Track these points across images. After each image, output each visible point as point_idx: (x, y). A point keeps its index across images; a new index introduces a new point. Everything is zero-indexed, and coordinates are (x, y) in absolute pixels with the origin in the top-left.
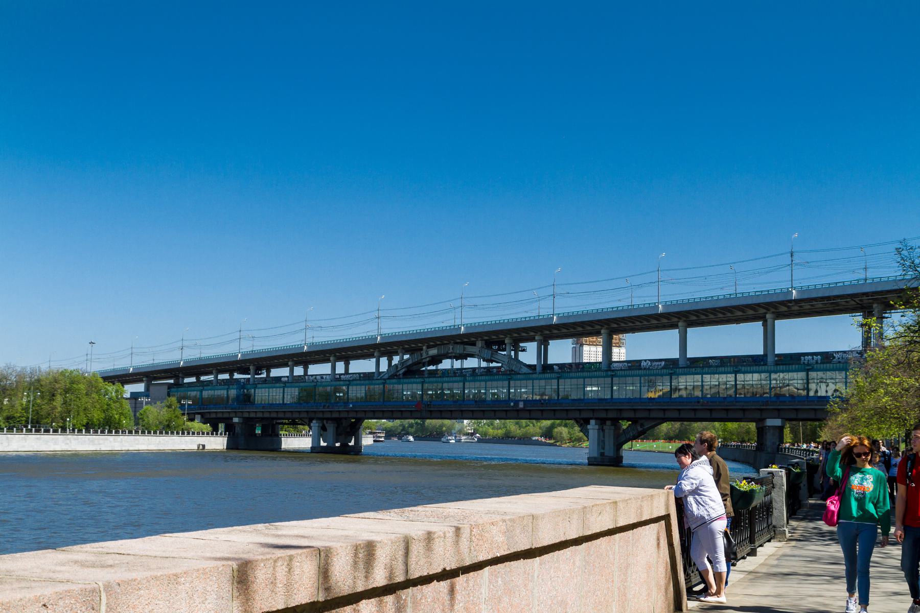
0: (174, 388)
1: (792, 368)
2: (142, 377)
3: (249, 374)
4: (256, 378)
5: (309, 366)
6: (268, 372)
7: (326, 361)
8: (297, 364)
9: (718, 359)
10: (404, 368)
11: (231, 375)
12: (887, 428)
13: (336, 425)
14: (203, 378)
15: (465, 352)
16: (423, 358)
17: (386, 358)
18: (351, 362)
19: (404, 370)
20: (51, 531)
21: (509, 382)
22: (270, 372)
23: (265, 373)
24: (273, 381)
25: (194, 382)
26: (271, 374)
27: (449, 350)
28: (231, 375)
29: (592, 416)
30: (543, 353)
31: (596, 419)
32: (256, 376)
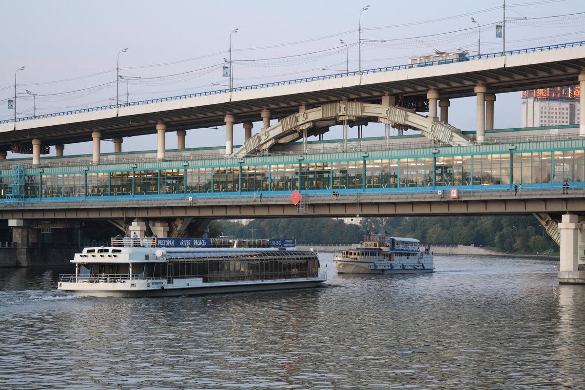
10: (270, 140)
13: (168, 229)
15: (364, 114)
16: (299, 123)
19: (270, 143)
22: (252, 126)
27: (340, 111)
29: (564, 209)
31: (572, 213)
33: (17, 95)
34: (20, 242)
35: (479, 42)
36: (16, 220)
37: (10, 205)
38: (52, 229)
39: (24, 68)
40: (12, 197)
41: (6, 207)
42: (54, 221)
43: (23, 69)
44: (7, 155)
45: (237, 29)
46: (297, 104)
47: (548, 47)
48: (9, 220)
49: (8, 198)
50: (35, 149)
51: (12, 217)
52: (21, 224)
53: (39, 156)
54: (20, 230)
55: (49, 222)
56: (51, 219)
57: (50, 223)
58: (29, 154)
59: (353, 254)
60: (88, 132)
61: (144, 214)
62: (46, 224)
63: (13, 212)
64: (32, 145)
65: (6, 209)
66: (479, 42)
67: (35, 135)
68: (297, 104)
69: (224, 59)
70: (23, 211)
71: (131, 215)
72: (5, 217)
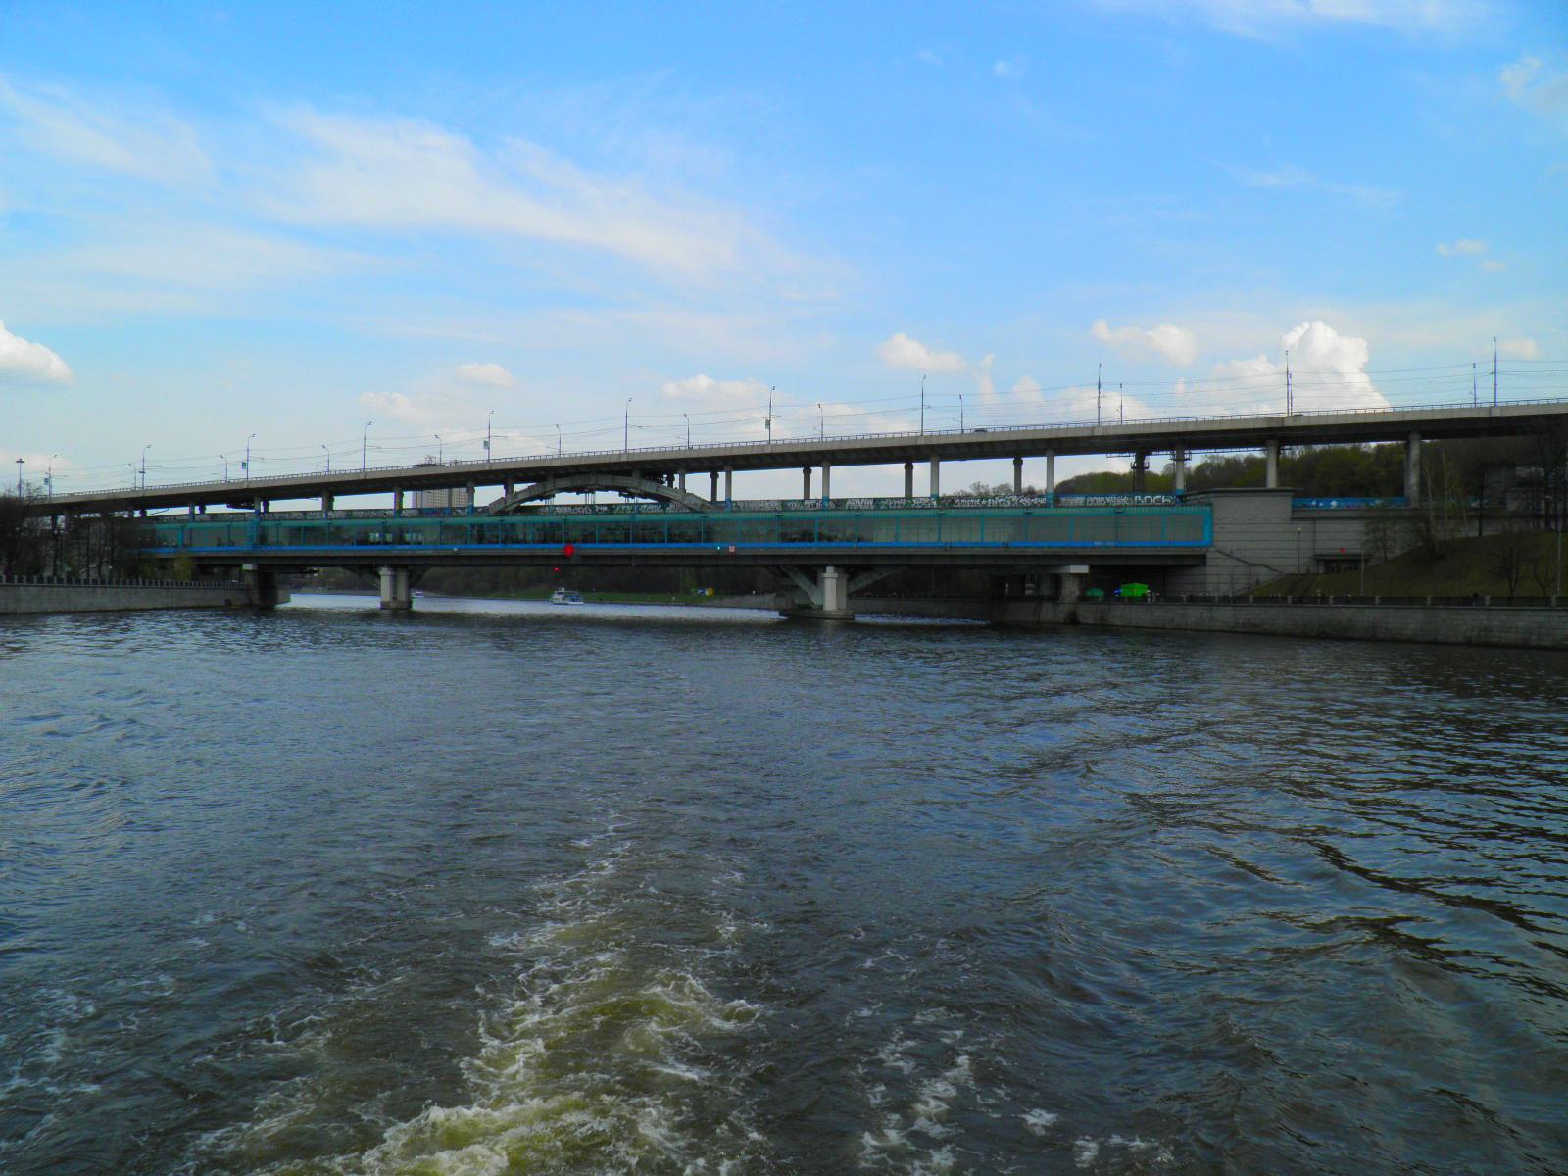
22: (333, 500)
31: (833, 566)
61: (395, 562)
63: (247, 559)
71: (824, 562)
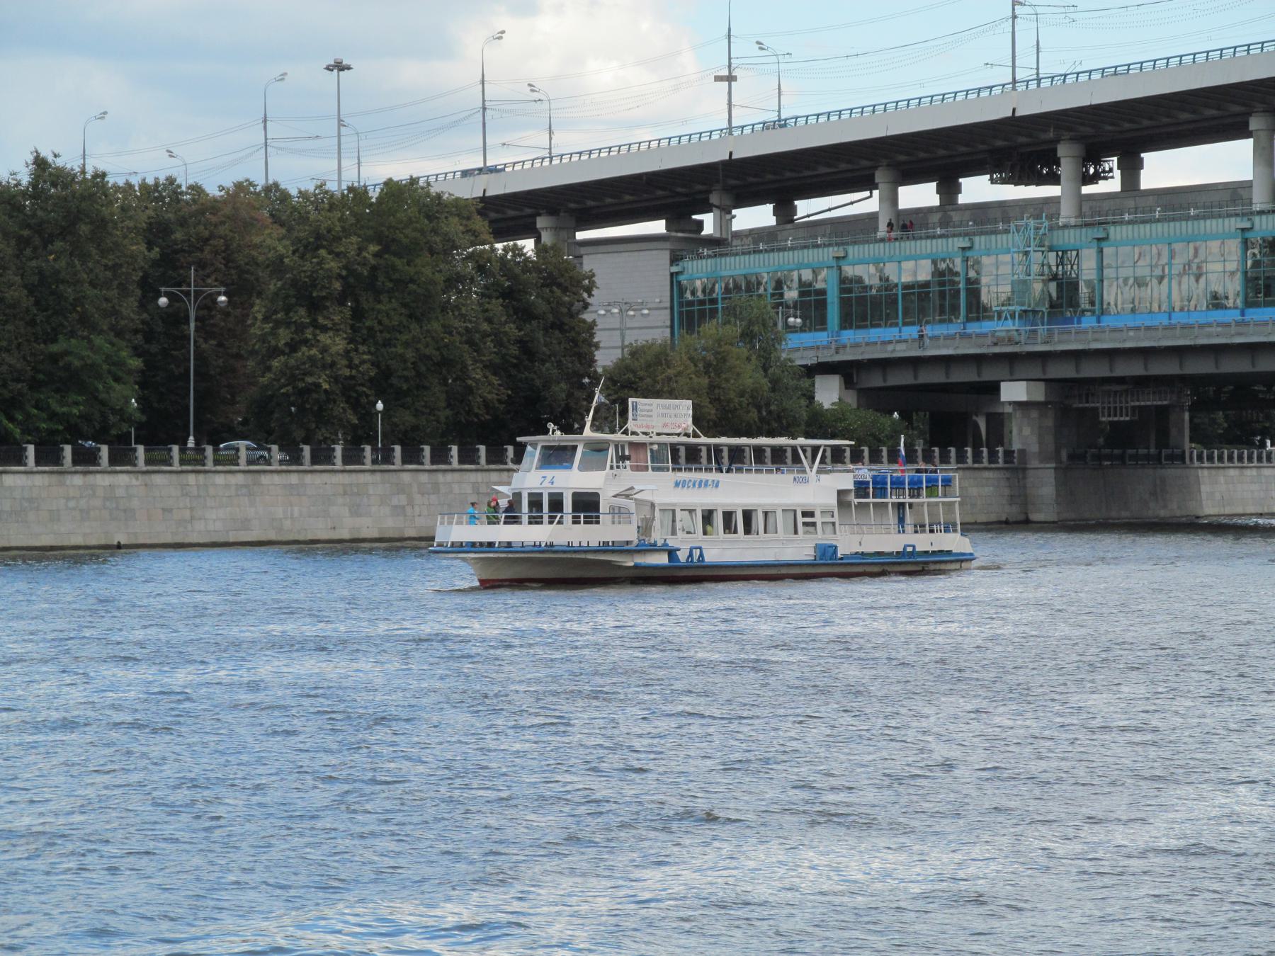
0: (700, 257)
1: (1199, 229)
2: (528, 211)
3: (1054, 179)
4: (1091, 197)
5: (1145, 156)
6: (1131, 168)
7: (866, 183)
8: (913, 176)
9: (747, 236)
11: (949, 189)
12: (496, 284)
14: (806, 208)
17: (934, 185)
18: (1149, 158)
20: (68, 772)
21: (1101, 251)
22: (1139, 165)
23: (1117, 173)
24: (756, 242)
25: (930, 210)
26: (1144, 174)
28: (949, 189)
30: (724, 222)
32: (1086, 190)
33: (1017, 12)
34: (1034, 448)
35: (779, 89)
36: (1025, 383)
37: (1011, 341)
38: (1134, 408)
39: (286, 77)
40: (1013, 316)
41: (996, 344)
42: (1141, 383)
43: (500, 38)
44: (959, 191)
45: (503, 32)
46: (1243, 109)
47: (1246, 48)
48: (1002, 384)
49: (999, 318)
50: (1066, 168)
51: (1011, 374)
52: (1039, 393)
53: (1080, 190)
54: (1034, 414)
55: (1125, 387)
56: (1133, 377)
57: (1126, 391)
58: (1038, 185)
59: (780, 519)
60: (700, 192)
62: (1116, 393)
63: (1013, 362)
64: (1059, 159)
65: (997, 350)
66: (779, 89)
67: (1070, 129)
68: (1243, 109)
69: (530, 85)
70: (1044, 357)
72: (988, 375)
